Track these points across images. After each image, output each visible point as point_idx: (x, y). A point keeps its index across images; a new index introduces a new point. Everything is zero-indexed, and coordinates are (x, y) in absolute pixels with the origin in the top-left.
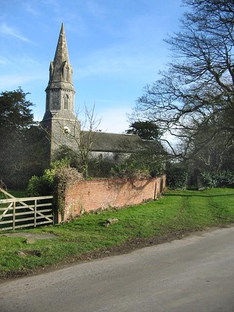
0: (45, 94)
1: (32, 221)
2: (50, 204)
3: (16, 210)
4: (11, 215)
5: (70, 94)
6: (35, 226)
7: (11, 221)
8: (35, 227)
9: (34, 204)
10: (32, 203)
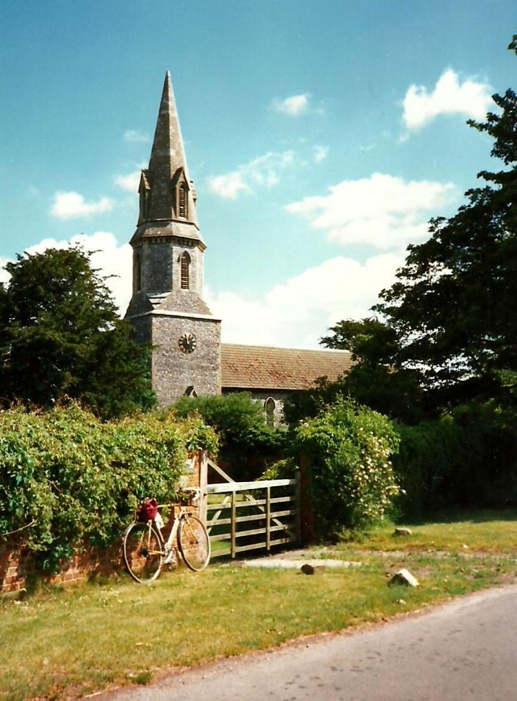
0: (129, 251)
1: (261, 538)
2: (287, 499)
3: (272, 504)
4: (228, 521)
5: (195, 252)
6: (234, 556)
7: (262, 531)
8: (233, 559)
9: (266, 498)
10: (260, 494)
